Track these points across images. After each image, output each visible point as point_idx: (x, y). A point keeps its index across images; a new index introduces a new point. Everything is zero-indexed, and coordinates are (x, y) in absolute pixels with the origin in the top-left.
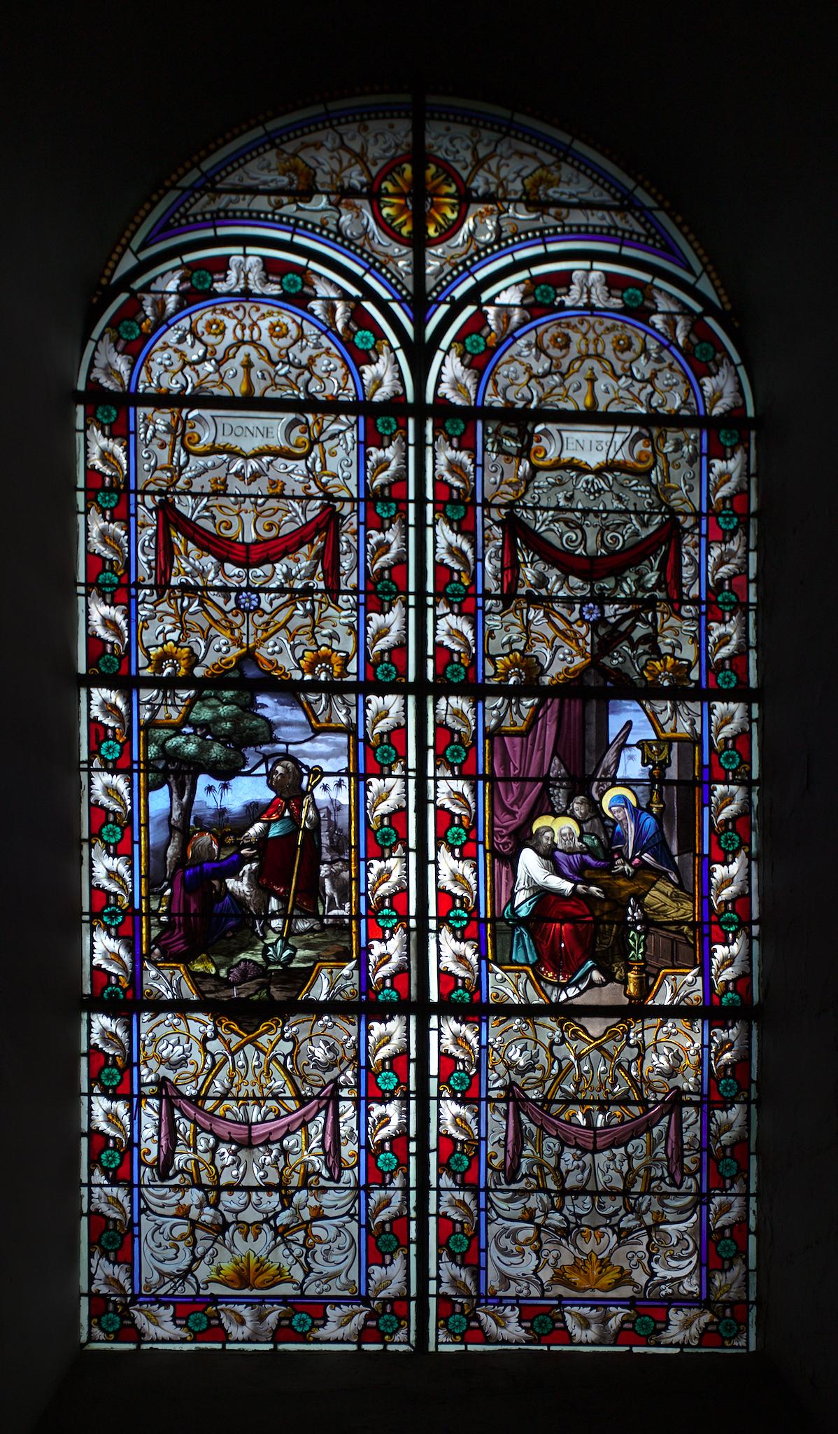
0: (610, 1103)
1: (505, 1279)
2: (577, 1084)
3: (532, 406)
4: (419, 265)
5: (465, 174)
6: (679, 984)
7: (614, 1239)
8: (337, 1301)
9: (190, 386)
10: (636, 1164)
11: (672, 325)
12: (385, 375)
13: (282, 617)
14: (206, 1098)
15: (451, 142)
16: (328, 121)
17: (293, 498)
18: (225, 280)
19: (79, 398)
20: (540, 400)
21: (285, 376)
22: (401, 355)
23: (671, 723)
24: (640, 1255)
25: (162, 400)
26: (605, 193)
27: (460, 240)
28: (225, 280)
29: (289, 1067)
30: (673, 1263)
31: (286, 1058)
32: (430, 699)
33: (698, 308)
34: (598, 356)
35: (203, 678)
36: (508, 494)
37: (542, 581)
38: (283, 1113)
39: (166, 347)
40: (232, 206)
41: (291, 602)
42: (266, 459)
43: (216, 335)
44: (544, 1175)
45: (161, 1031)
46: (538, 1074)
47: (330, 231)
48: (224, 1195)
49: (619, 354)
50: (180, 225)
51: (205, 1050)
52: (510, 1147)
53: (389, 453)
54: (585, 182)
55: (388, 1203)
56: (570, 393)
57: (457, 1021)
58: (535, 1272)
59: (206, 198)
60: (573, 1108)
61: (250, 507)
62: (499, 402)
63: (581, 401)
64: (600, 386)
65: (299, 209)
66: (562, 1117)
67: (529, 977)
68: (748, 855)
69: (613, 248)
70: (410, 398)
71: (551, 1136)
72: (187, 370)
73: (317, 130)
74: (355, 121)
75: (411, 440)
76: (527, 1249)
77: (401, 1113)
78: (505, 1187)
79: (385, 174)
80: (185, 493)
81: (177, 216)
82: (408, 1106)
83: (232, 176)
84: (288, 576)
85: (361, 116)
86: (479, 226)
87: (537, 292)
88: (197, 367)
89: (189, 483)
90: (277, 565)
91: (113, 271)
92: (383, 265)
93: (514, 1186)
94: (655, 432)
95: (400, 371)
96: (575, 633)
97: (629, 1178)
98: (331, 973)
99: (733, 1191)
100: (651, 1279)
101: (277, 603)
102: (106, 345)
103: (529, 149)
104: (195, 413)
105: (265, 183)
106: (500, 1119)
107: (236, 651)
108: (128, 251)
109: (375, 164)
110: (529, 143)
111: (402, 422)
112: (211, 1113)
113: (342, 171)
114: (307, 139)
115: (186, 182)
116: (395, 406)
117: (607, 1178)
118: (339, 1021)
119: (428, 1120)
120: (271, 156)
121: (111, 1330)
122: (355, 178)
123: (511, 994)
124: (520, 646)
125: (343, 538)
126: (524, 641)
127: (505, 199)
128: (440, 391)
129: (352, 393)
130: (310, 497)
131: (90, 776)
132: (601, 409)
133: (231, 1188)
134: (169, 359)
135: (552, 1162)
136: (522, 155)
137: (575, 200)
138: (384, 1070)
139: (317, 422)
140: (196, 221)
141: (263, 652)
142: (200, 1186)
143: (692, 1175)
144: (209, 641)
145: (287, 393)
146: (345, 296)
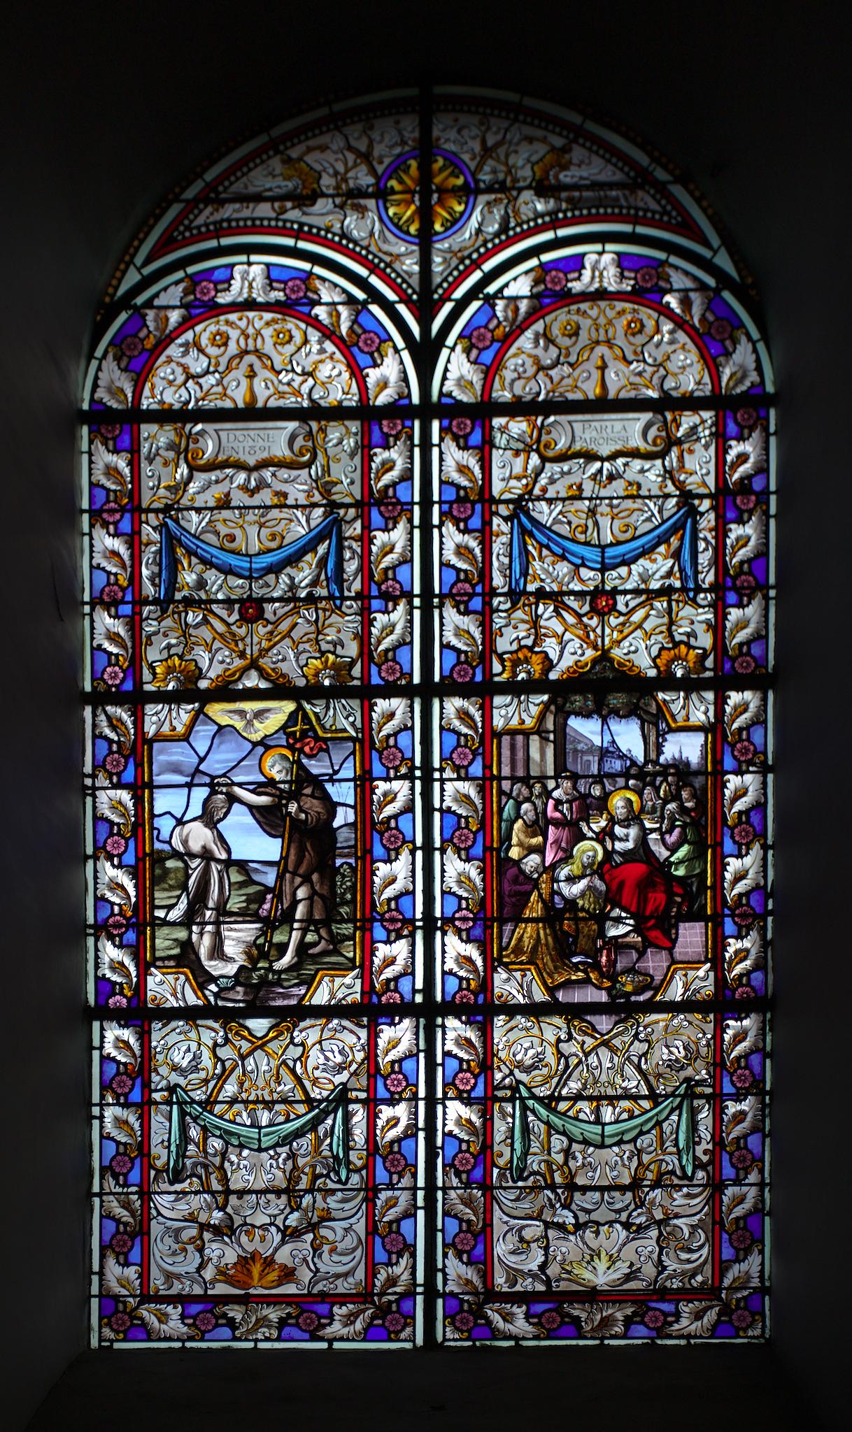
0: (274, 1102)
1: (169, 1277)
2: (241, 1084)
3: (190, 407)
4: (425, 262)
5: (472, 165)
6: (690, 978)
7: (278, 1238)
8: (343, 1299)
9: (543, 392)
10: (301, 1162)
11: (686, 303)
12: (391, 373)
13: (637, 617)
14: (561, 1098)
15: (459, 132)
16: (335, 122)
17: (296, 507)
18: (579, 279)
19: (84, 417)
20: (197, 401)
21: (289, 384)
22: (406, 355)
23: (683, 713)
24: (305, 1252)
25: (164, 416)
26: (618, 172)
27: (467, 235)
28: (579, 279)
29: (299, 1070)
30: (684, 1256)
31: (295, 1061)
32: (436, 703)
33: (711, 282)
34: (609, 343)
35: (207, 690)
36: (517, 487)
37: (201, 584)
38: (637, 1113)
39: (170, 360)
40: (236, 216)
41: (295, 611)
42: (620, 461)
43: (219, 346)
44: (208, 1174)
45: (172, 1039)
46: (545, 1071)
47: (334, 234)
48: (577, 1195)
49: (631, 338)
50: (184, 237)
51: (215, 1056)
52: (173, 1148)
53: (394, 454)
54: (597, 162)
55: (742, 1200)
56: (229, 392)
57: (120, 1026)
58: (199, 1270)
59: (209, 209)
60: (580, 1104)
61: (606, 510)
62: (507, 396)
63: (591, 390)
64: (611, 375)
65: (304, 214)
66: (226, 1117)
67: (187, 979)
68: (765, 847)
69: (627, 228)
70: (416, 399)
71: (214, 1135)
72: (190, 384)
73: (322, 133)
74: (360, 120)
75: (417, 441)
76: (190, 1248)
77: (410, 1113)
78: (511, 1184)
79: (393, 171)
80: (539, 499)
81: (182, 228)
82: (416, 1107)
83: (235, 185)
84: (645, 578)
85: (368, 116)
86: (480, 219)
87: (548, 278)
88: (201, 381)
89: (544, 490)
90: (633, 567)
91: (116, 289)
92: (388, 265)
93: (520, 1184)
94: (669, 416)
95: (405, 372)
96: (234, 635)
97: (293, 1179)
98: (685, 975)
99: (400, 1185)
100: (660, 1273)
101: (632, 604)
102: (110, 365)
103: (539, 133)
104: (199, 427)
105: (270, 190)
106: (163, 1120)
107: (590, 653)
108: (132, 268)
109: (381, 162)
110: (539, 127)
111: (762, 413)
112: (564, 1114)
113: (347, 171)
114: (311, 143)
115: (190, 194)
116: (399, 410)
117: (615, 1173)
118: (346, 1023)
119: (435, 1117)
120: (276, 164)
121: (465, 1328)
122: (365, 179)
123: (169, 997)
124: (529, 642)
125: (701, 535)
126: (532, 637)
127: (513, 188)
128: (97, 396)
129: (356, 398)
130: (667, 496)
131: (151, 794)
132: (260, 404)
133: (584, 1189)
134: (523, 365)
135: (217, 1161)
136: (530, 140)
137: (587, 182)
138: (740, 1067)
139: (320, 429)
140: (200, 232)
141: (617, 653)
142: (553, 1187)
143: (358, 1171)
144: (563, 645)
145: (290, 402)
146: (702, 287)
